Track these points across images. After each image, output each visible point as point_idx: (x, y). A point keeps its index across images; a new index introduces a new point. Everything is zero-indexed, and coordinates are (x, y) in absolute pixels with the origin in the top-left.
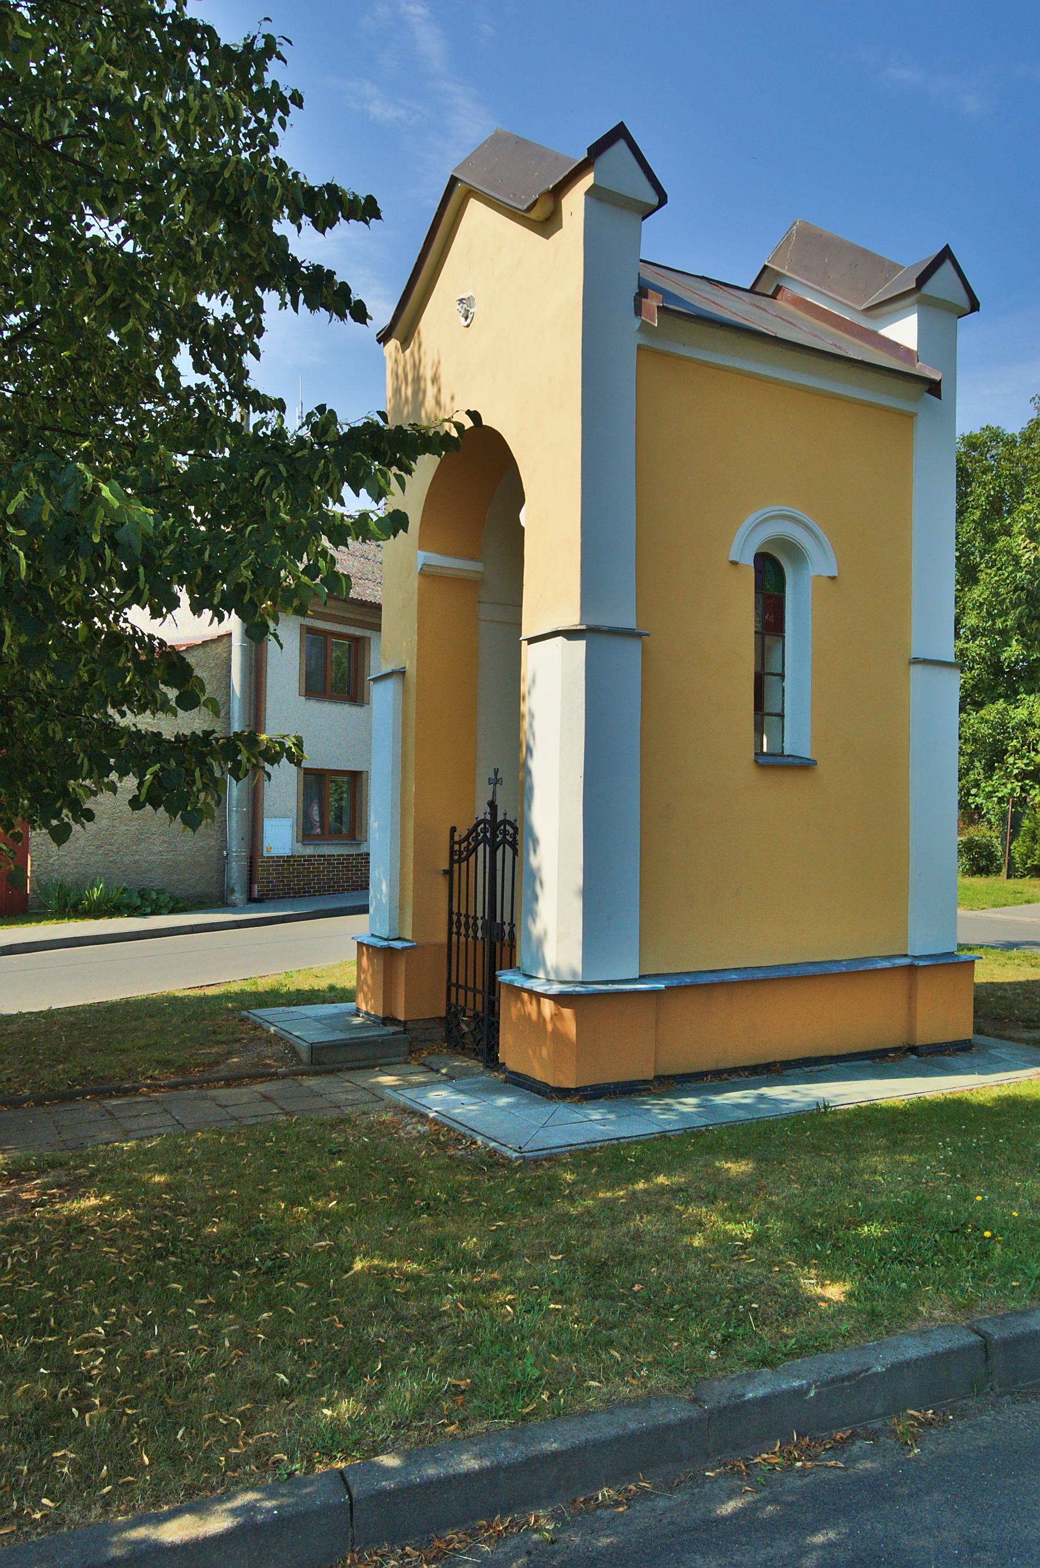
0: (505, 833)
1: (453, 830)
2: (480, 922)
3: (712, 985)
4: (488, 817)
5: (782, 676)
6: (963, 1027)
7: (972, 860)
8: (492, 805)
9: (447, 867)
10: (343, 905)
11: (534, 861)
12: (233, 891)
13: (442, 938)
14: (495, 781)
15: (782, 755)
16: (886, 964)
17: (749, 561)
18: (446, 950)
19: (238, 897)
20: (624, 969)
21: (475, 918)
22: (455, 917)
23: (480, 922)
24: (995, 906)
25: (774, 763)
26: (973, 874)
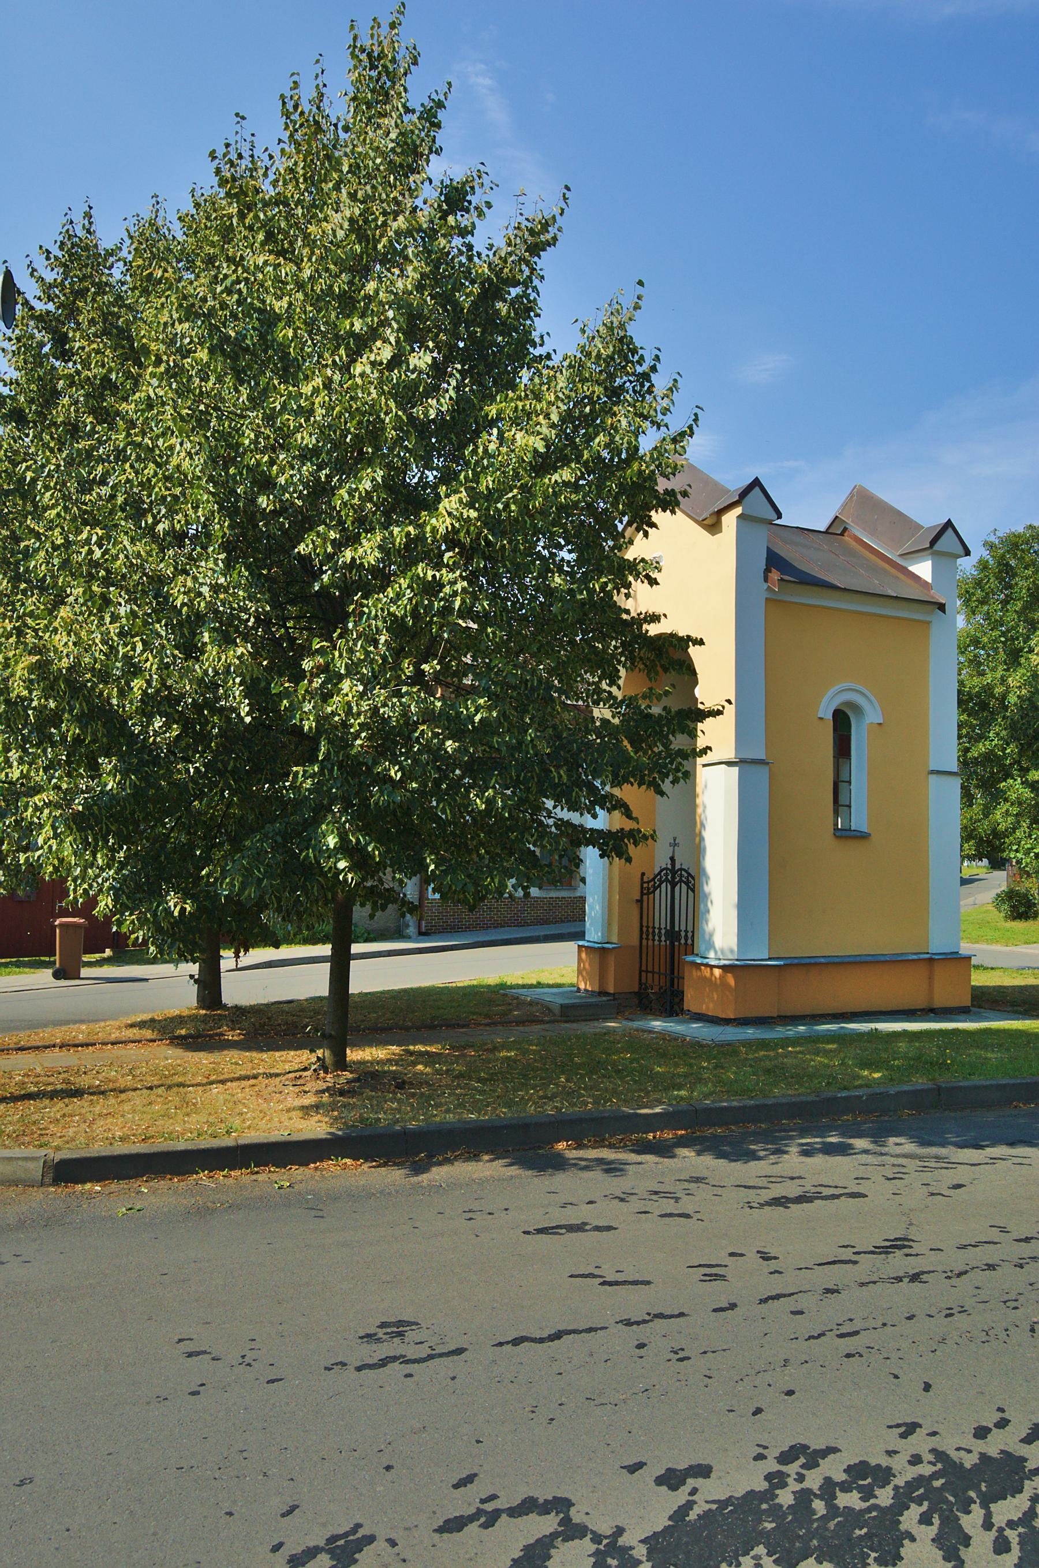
0: (681, 876)
1: (643, 874)
2: (663, 931)
3: (810, 964)
4: (669, 867)
5: (850, 782)
6: (967, 1001)
7: (1013, 907)
8: (672, 859)
9: (639, 898)
10: (493, 938)
11: (706, 889)
12: (408, 926)
13: (635, 942)
14: (674, 844)
15: (850, 830)
16: (915, 957)
17: (829, 716)
18: (638, 952)
19: (412, 930)
20: (760, 953)
21: (660, 929)
22: (645, 929)
23: (663, 931)
24: (1026, 943)
25: (846, 835)
26: (1014, 919)
